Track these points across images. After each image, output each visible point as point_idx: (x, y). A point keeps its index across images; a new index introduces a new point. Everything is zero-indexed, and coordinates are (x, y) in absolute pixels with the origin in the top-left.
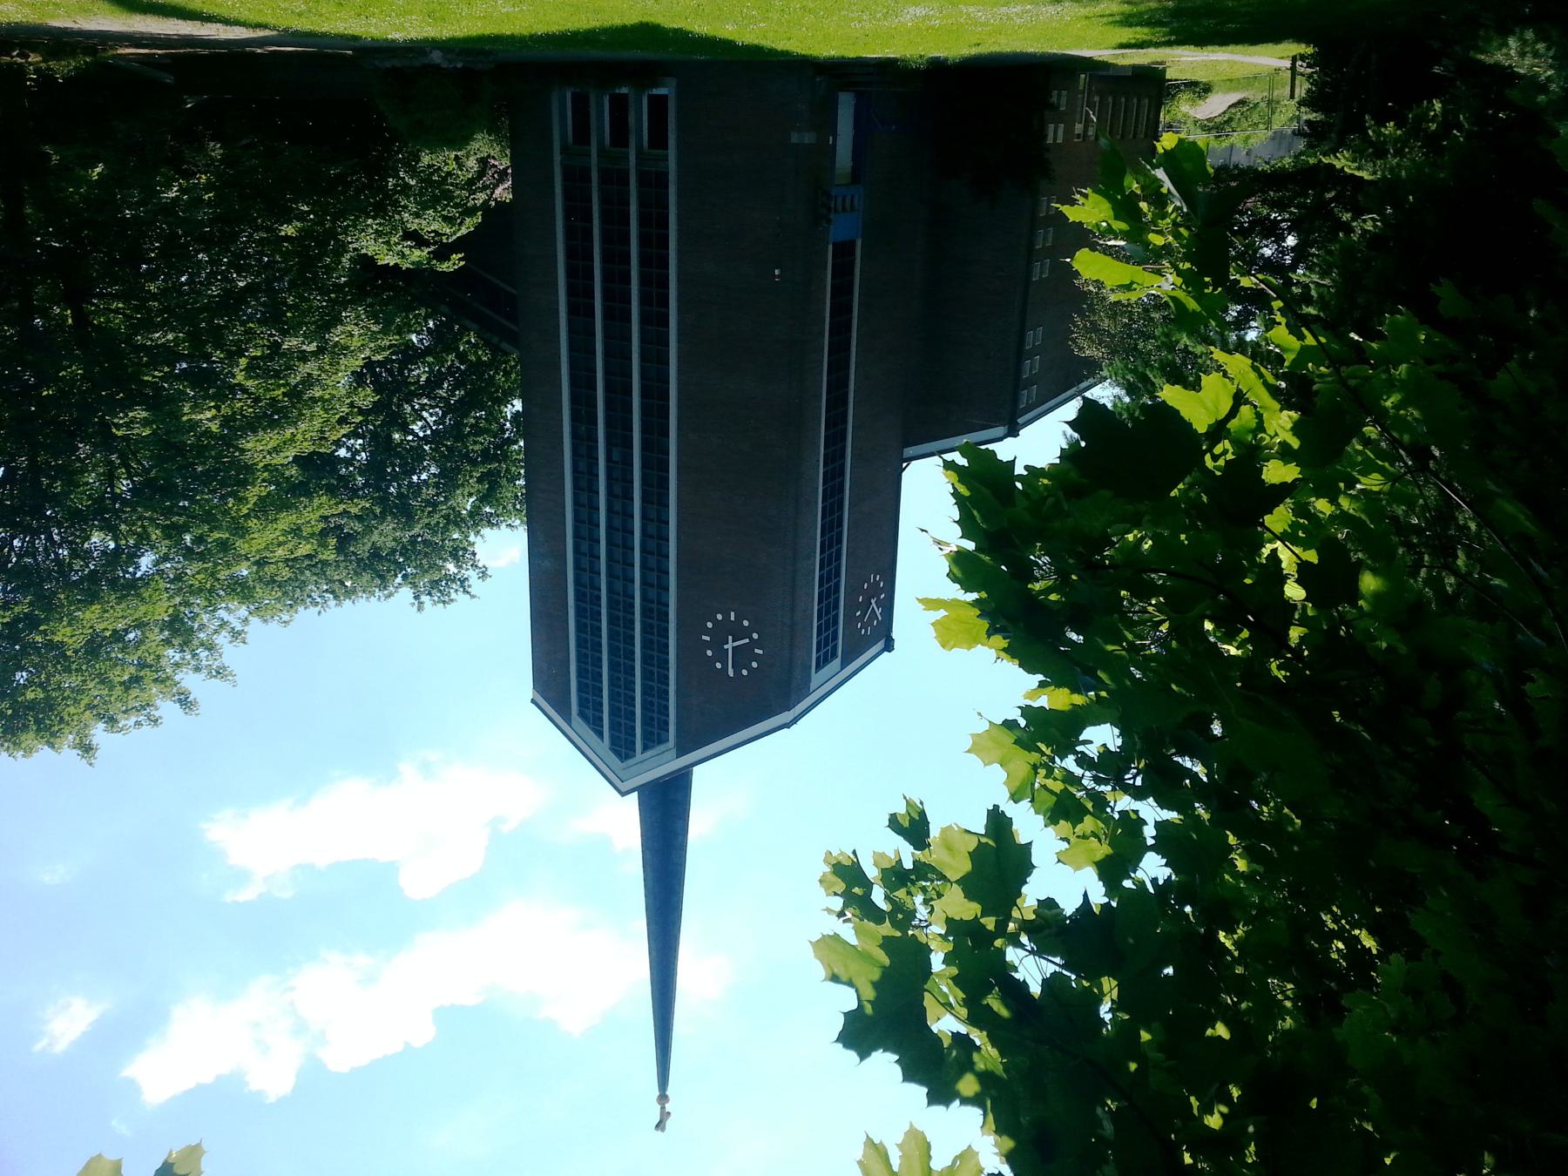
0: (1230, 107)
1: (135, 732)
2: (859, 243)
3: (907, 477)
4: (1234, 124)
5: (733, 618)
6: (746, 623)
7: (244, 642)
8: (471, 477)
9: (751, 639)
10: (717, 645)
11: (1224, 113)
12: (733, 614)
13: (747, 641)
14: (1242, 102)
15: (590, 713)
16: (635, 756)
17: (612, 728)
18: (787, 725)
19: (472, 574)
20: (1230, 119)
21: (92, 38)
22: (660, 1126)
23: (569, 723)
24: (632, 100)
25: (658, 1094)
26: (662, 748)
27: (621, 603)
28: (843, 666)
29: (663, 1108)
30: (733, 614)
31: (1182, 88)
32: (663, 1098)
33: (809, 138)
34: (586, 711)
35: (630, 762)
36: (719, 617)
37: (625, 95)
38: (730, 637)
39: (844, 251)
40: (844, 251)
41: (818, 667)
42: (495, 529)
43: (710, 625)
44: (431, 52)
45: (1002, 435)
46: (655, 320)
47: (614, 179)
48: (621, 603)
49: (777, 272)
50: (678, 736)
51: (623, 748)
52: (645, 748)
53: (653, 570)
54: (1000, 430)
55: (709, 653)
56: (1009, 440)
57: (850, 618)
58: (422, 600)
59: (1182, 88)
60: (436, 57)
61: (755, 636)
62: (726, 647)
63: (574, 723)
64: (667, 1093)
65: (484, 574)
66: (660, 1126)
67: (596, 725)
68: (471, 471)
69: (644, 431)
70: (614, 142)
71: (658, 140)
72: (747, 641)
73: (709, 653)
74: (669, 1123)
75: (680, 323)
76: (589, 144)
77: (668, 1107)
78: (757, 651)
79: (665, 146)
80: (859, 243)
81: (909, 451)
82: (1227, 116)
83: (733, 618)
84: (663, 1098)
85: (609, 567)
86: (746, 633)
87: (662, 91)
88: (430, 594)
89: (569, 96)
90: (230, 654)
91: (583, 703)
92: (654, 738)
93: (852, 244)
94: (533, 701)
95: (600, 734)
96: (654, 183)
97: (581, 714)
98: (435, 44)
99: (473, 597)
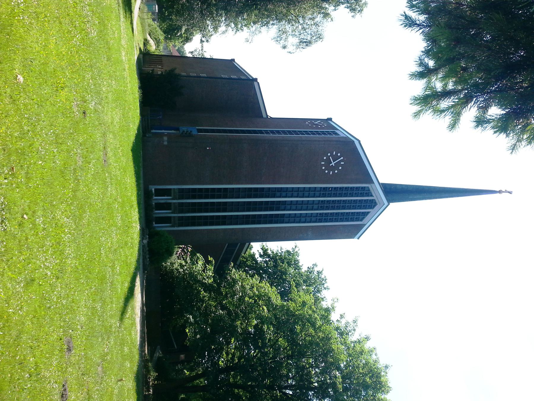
0: (151, 38)
1: (379, 355)
2: (197, 128)
3: (273, 116)
4: (156, 37)
5: (324, 163)
6: (325, 158)
7: (344, 314)
8: (282, 266)
9: (330, 156)
10: (333, 168)
11: (153, 40)
12: (322, 163)
13: (330, 157)
14: (150, 35)
15: (361, 217)
16: (375, 200)
17: (366, 209)
18: (359, 141)
19: (316, 269)
20: (155, 38)
21: (140, 253)
22: (510, 193)
23: (365, 225)
24: (156, 202)
25: (498, 194)
26: (371, 189)
27: (322, 205)
28: (338, 130)
29: (504, 192)
30: (322, 163)
31: (146, 48)
32: (500, 192)
33: (165, 138)
34: (360, 218)
35: (377, 201)
36: (323, 168)
37: (155, 203)
38: (330, 165)
39: (199, 131)
40: (199, 131)
41: (339, 135)
42: (300, 261)
43: (326, 172)
44: (144, 243)
45: (257, 83)
46: (225, 193)
47: (182, 208)
48: (322, 205)
49: (208, 148)
50: (366, 183)
51: (372, 204)
52: (372, 196)
53: (309, 193)
54: (255, 83)
55: (336, 171)
56: (258, 81)
57: (319, 128)
58: (326, 287)
59: (146, 48)
60: (145, 241)
61: (329, 154)
62: (334, 165)
63: (365, 223)
64: (498, 191)
65: (315, 265)
66: (510, 193)
67: (366, 214)
68: (280, 266)
69: (262, 197)
70: (169, 195)
71: (167, 192)
72: (330, 157)
73: (336, 171)
74: (509, 190)
75: (226, 184)
76: (171, 189)
77: (504, 190)
78: (334, 154)
79: (170, 190)
80: (197, 128)
81: (264, 116)
82: (154, 39)
83: (324, 163)
84: (500, 192)
85: (309, 210)
86: (328, 158)
87: (153, 190)
88: (324, 284)
89: (157, 211)
90: (349, 318)
91: (357, 220)
92: (369, 194)
93: (198, 129)
94: (358, 239)
95: (368, 213)
96: (183, 193)
97: (361, 220)
98: (141, 242)
99: (323, 269)
